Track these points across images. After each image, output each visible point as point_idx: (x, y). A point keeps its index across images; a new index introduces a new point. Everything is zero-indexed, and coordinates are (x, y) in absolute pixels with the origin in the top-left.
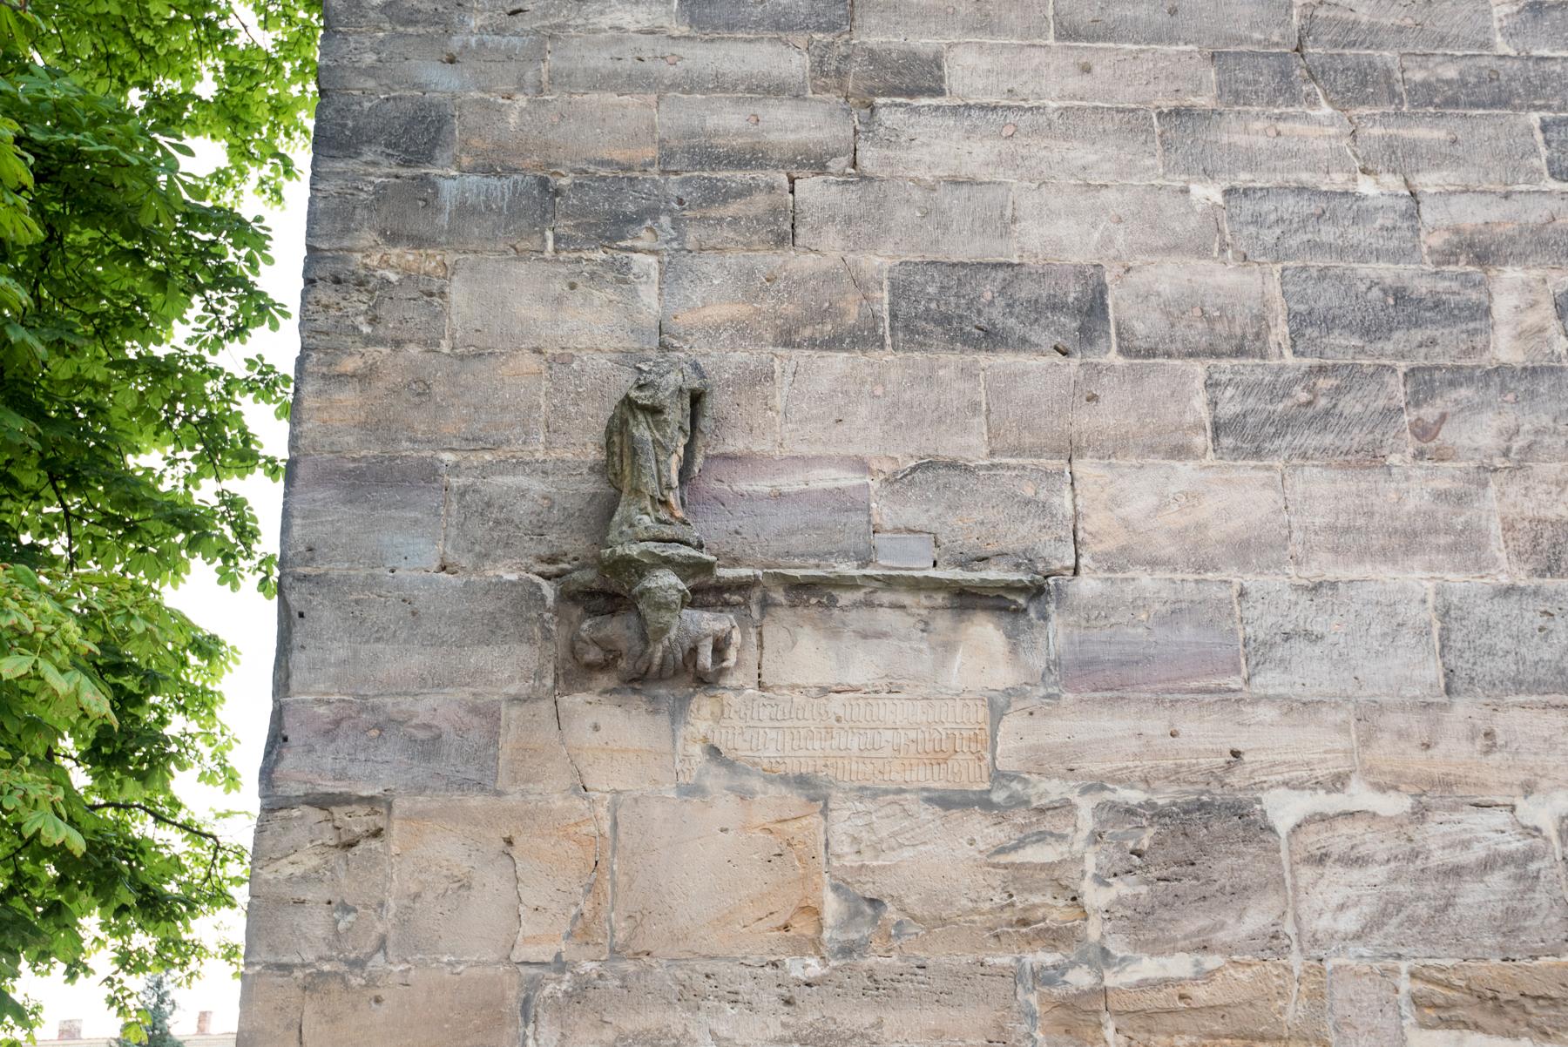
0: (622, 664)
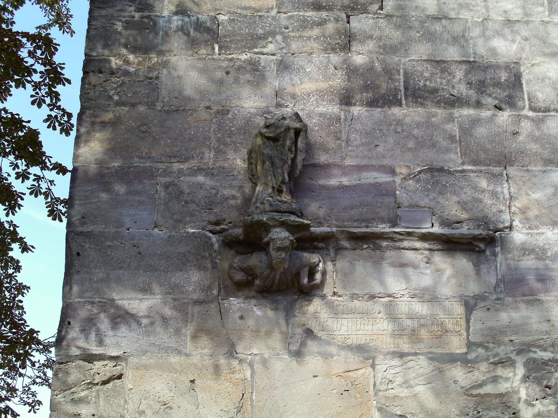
0: (257, 282)
